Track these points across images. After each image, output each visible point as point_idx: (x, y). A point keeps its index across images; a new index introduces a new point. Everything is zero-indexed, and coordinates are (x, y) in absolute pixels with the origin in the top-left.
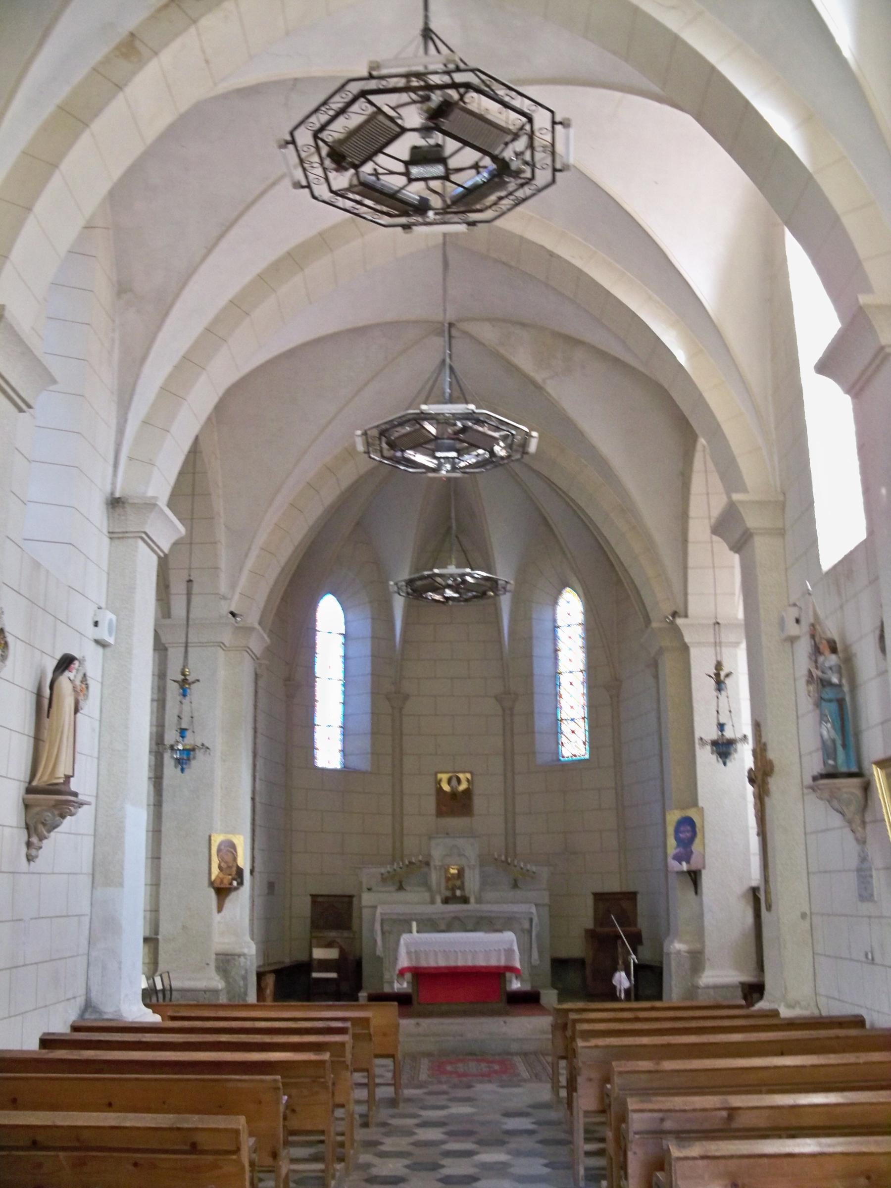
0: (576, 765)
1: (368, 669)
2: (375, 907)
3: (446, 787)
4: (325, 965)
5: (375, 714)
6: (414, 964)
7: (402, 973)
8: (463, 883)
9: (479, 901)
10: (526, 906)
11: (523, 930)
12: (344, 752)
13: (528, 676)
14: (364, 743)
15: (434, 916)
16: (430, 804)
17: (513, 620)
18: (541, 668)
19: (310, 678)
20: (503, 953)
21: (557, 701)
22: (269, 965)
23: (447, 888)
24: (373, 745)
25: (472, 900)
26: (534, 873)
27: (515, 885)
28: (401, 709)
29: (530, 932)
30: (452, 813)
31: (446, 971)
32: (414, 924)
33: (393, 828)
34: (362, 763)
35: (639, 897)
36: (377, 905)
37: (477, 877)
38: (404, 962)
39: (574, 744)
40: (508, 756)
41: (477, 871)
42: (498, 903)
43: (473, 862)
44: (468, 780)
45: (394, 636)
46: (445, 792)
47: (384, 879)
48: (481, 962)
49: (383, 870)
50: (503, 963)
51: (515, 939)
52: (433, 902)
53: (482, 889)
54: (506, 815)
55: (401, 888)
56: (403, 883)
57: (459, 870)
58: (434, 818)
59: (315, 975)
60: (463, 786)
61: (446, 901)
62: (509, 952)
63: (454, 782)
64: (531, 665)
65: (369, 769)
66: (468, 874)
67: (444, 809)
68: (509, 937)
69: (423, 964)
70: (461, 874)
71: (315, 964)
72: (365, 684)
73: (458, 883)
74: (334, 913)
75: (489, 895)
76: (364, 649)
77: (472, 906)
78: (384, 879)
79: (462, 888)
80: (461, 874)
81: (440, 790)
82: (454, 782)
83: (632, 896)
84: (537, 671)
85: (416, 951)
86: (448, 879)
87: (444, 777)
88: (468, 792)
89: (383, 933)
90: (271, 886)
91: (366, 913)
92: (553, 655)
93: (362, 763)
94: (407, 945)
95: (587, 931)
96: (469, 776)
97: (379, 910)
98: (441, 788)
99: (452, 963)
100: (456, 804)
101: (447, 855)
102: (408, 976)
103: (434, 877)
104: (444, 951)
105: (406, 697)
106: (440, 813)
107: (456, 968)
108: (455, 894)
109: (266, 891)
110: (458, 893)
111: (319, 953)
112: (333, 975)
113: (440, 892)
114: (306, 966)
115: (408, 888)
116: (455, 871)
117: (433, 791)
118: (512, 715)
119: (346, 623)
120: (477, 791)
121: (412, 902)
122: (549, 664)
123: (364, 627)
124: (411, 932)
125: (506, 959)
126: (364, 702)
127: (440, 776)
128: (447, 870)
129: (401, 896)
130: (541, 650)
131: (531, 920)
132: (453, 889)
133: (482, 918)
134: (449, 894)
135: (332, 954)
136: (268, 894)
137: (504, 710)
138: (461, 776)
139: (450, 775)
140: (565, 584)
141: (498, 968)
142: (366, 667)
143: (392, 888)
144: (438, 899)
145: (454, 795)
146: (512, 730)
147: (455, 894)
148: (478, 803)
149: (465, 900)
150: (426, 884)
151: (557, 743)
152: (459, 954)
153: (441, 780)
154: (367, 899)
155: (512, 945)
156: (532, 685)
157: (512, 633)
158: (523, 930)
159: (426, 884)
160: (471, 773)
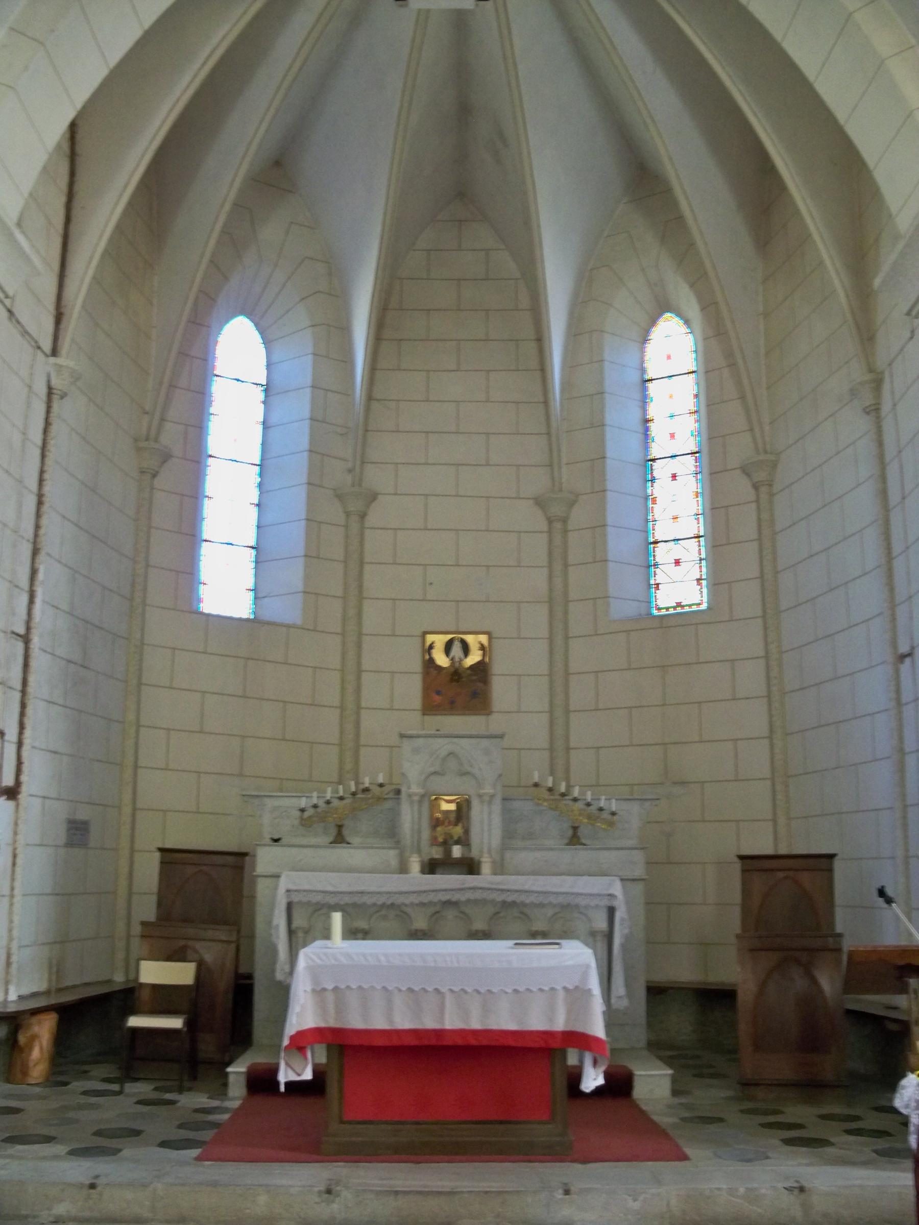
0: (680, 621)
1: (305, 443)
2: (277, 876)
3: (442, 660)
4: (164, 998)
5: (313, 523)
6: (332, 1023)
7: (300, 1043)
8: (467, 831)
9: (500, 868)
10: (602, 882)
11: (593, 934)
12: (258, 593)
13: (597, 461)
14: (293, 575)
15: (400, 900)
16: (412, 689)
17: (570, 365)
18: (620, 447)
19: (195, 459)
20: (561, 994)
21: (647, 510)
22: (59, 990)
23: (434, 842)
24: (307, 578)
25: (486, 868)
26: (613, 814)
27: (574, 839)
28: (363, 516)
29: (609, 936)
30: (451, 707)
31: (413, 1042)
32: (337, 918)
33: (342, 732)
34: (287, 610)
35: (837, 864)
36: (285, 875)
37: (497, 820)
38: (303, 1015)
39: (680, 583)
40: (557, 604)
41: (497, 807)
42: (535, 873)
43: (488, 790)
44: (482, 648)
45: (354, 390)
46: (439, 668)
47: (308, 820)
48: (504, 1020)
49: (303, 803)
50: (560, 1025)
51: (593, 964)
52: (403, 869)
53: (505, 847)
54: (551, 712)
55: (340, 839)
56: (345, 832)
57: (459, 806)
58: (418, 714)
59: (135, 1021)
60: (474, 658)
61: (431, 867)
62: (577, 996)
63: (457, 650)
64: (601, 442)
65: (299, 622)
66: (477, 812)
67: (438, 699)
68: (576, 957)
69: (356, 1022)
70: (462, 814)
71: (145, 995)
72: (297, 467)
73: (458, 831)
74: (206, 891)
75: (525, 858)
76: (298, 407)
77: (486, 877)
78: (308, 820)
79: (464, 841)
80: (462, 814)
81: (430, 664)
82: (457, 650)
83: (824, 862)
84: (611, 451)
85: (336, 989)
86: (436, 824)
87: (440, 640)
88: (481, 669)
89: (291, 932)
90: (77, 832)
91: (262, 887)
92: (640, 429)
93: (287, 610)
94: (315, 972)
95: (738, 936)
96: (484, 639)
97: (284, 884)
98: (431, 661)
99: (429, 1023)
100: (459, 689)
101: (435, 773)
102: (319, 1054)
103: (409, 818)
104: (410, 990)
105: (373, 497)
106: (429, 708)
107: (439, 1033)
108: (450, 856)
109: (62, 840)
110: (457, 851)
111: (155, 973)
112: (175, 1023)
113: (419, 851)
114: (129, 997)
115: (356, 840)
116: (452, 807)
117: (417, 665)
118: (565, 531)
119: (269, 366)
120: (497, 668)
121: (364, 868)
122: (635, 440)
123: (300, 368)
124: (327, 936)
125: (569, 1012)
126: (294, 501)
127: (430, 638)
128: (434, 805)
129: (342, 854)
130: (619, 415)
131: (611, 911)
132: (446, 844)
133: (505, 905)
134: (437, 853)
135: (180, 974)
136: (69, 844)
137: (550, 521)
138: (469, 639)
139: (450, 636)
140: (663, 306)
141: (548, 1035)
142: (298, 437)
143: (325, 840)
144: (415, 866)
145: (456, 674)
146: (565, 558)
147: (450, 856)
148: (501, 690)
149: (470, 867)
150: (392, 833)
151: (650, 587)
152: (449, 1001)
153: (431, 647)
154: (266, 860)
155: (585, 976)
156: (603, 474)
157: (567, 385)
158: (593, 934)
159: (392, 833)
160: (488, 633)
